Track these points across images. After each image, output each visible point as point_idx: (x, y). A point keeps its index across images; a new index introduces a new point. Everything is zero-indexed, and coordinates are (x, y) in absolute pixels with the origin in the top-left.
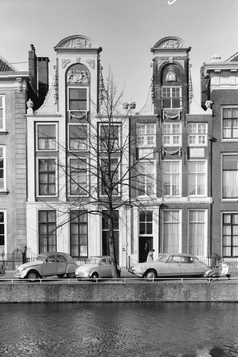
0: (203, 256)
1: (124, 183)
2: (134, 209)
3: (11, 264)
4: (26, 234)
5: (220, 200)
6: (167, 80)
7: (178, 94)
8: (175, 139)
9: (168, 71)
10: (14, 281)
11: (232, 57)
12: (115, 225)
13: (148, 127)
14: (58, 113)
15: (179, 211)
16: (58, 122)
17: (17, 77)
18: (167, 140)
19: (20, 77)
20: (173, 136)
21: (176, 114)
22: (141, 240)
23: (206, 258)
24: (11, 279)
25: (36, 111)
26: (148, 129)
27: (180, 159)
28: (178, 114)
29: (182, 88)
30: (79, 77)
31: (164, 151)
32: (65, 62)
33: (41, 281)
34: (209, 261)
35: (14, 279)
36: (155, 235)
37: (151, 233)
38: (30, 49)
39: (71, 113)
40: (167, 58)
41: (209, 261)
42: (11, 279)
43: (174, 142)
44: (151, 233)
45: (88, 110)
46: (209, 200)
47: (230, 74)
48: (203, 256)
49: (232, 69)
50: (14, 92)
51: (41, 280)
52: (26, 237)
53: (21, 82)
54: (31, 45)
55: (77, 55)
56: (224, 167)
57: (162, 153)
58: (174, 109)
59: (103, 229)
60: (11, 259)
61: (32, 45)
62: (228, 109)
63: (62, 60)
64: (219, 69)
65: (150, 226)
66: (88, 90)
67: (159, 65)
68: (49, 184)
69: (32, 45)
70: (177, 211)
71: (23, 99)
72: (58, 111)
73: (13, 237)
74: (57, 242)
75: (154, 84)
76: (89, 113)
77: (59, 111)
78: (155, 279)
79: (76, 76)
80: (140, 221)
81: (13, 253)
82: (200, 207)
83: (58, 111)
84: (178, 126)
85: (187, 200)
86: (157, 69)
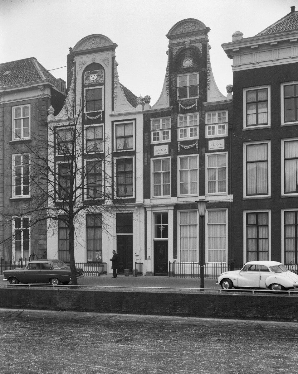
1: (41, 187)
2: (148, 211)
4: (46, 239)
8: (165, 134)
10: (255, 292)
12: (130, 228)
13: (164, 120)
15: (225, 211)
16: (135, 120)
17: (39, 86)
18: (166, 135)
19: (42, 85)
20: (219, 126)
21: (193, 104)
23: (197, 265)
24: (252, 290)
28: (195, 103)
29: (200, 74)
30: (94, 77)
33: (289, 294)
35: (254, 290)
36: (170, 239)
37: (167, 237)
40: (184, 43)
42: (252, 290)
43: (191, 135)
44: (167, 237)
45: (103, 110)
47: (290, 44)
49: (272, 42)
50: (37, 100)
51: (253, 291)
52: (46, 242)
55: (93, 55)
56: (286, 155)
57: (176, 148)
58: (191, 98)
62: (263, 90)
63: (79, 62)
64: (237, 48)
67: (174, 54)
68: (125, 185)
70: (215, 211)
73: (35, 242)
75: (170, 73)
76: (104, 113)
77: (115, 109)
78: (202, 289)
79: (92, 76)
80: (168, 225)
84: (196, 116)
85: (150, 202)
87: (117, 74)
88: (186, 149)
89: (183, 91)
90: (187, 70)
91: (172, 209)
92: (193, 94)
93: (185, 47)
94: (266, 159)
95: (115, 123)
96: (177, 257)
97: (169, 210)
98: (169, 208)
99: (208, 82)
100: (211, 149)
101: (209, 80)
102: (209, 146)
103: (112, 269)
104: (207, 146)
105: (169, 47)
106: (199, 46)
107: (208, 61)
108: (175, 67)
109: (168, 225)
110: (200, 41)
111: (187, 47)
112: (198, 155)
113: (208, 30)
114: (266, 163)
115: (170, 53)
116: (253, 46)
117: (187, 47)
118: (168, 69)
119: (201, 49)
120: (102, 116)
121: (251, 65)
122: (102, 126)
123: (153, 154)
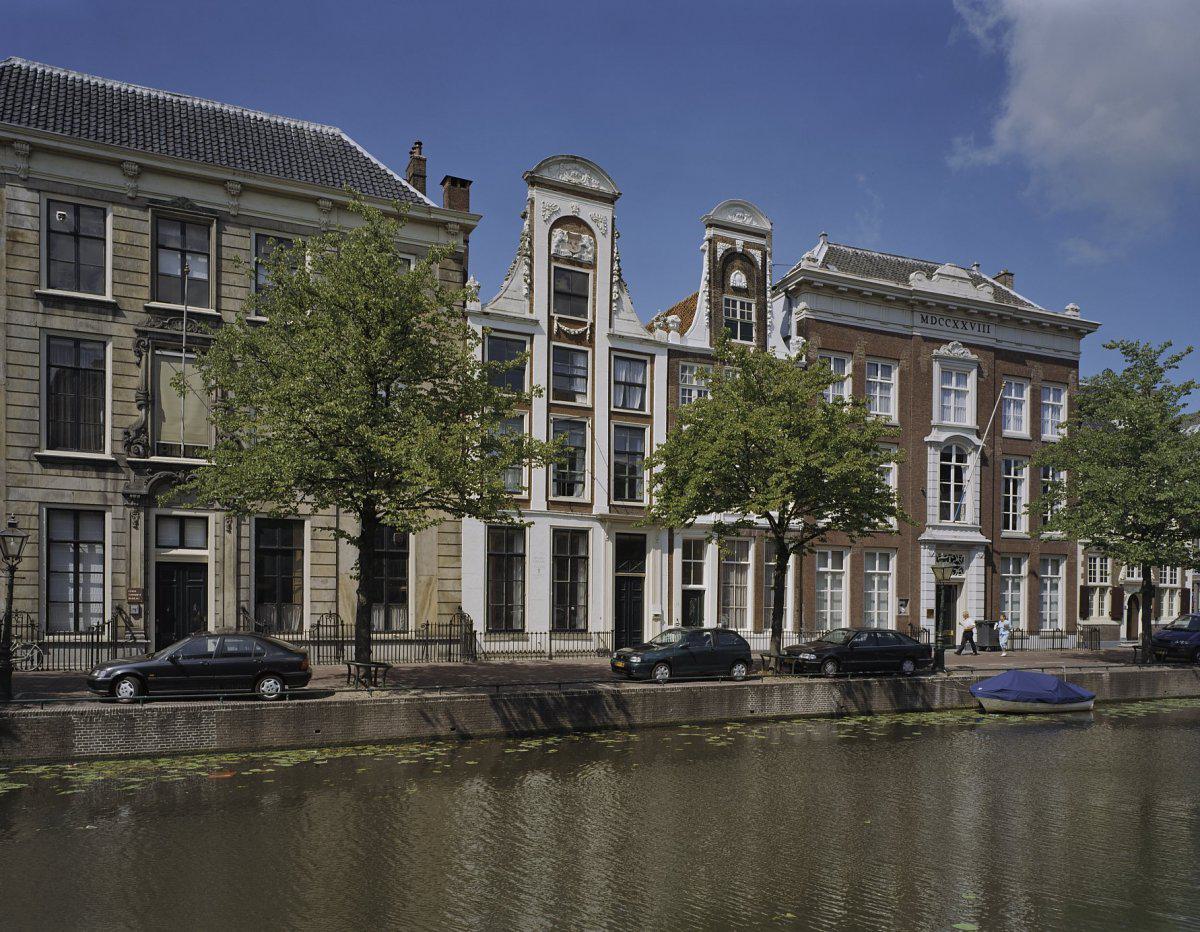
0: (745, 630)
7: (750, 315)
9: (733, 267)
14: (533, 317)
22: (686, 594)
26: (620, 574)
39: (560, 320)
48: (745, 630)
59: (617, 571)
65: (699, 568)
66: (591, 277)
71: (458, 273)
72: (531, 311)
74: (527, 597)
83: (531, 311)
86: (715, 258)
120: (588, 332)
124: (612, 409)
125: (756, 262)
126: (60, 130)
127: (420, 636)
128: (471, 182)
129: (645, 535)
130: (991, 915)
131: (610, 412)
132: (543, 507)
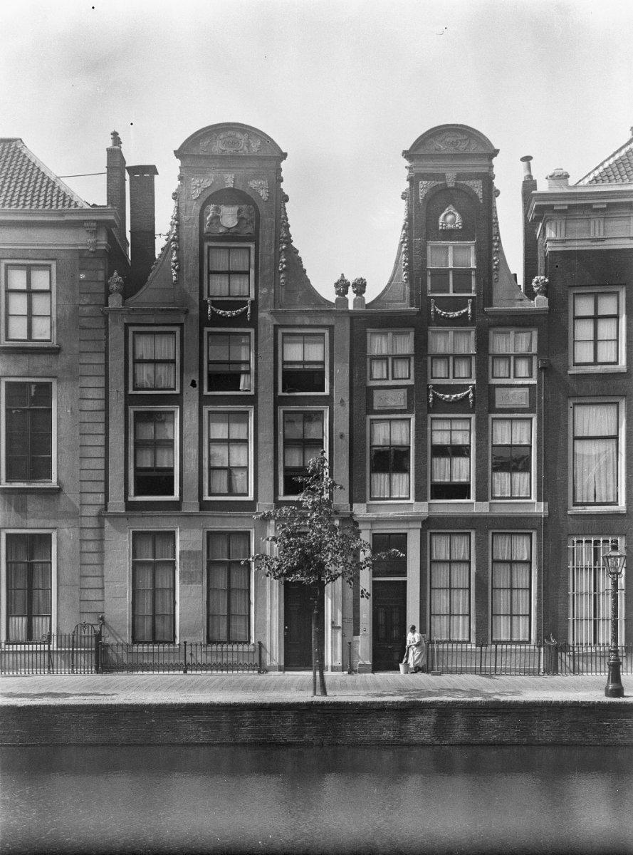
3: (42, 658)
5: (567, 509)
6: (440, 228)
11: (597, 168)
16: (181, 325)
19: (95, 221)
25: (130, 299)
27: (471, 413)
31: (433, 394)
32: (200, 187)
34: (481, 657)
38: (110, 144)
41: (481, 657)
46: (540, 509)
53: (95, 233)
54: (112, 134)
60: (90, 645)
61: (115, 134)
69: (115, 134)
81: (74, 632)
82: (516, 525)
86: (417, 199)
87: (287, 220)
88: (449, 403)
89: (441, 274)
90: (449, 234)
91: (418, 528)
92: (462, 284)
93: (446, 184)
94: (613, 433)
95: (280, 331)
96: (419, 503)
97: (410, 529)
98: (411, 525)
99: (495, 265)
100: (501, 407)
101: (496, 263)
102: (496, 400)
103: (536, 180)
104: (492, 399)
105: (410, 179)
106: (477, 187)
107: (494, 220)
108: (421, 228)
109: (406, 582)
110: (477, 176)
111: (449, 173)
112: (473, 417)
113: (496, 152)
114: (614, 441)
115: (410, 196)
116: (598, 204)
117: (451, 185)
118: (406, 227)
119: (479, 191)
121: (589, 243)
122: (249, 334)
123: (494, 406)
124: (131, 392)
125: (476, 195)
126: (608, 181)
127: (61, 647)
128: (115, 157)
129: (406, 534)
130: (40, 740)
131: (127, 396)
132: (196, 510)
